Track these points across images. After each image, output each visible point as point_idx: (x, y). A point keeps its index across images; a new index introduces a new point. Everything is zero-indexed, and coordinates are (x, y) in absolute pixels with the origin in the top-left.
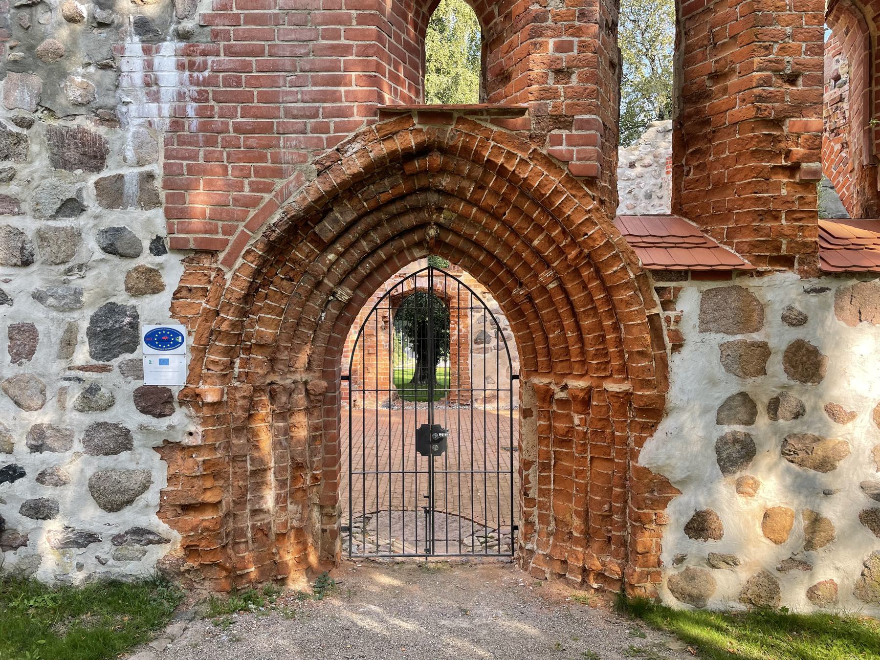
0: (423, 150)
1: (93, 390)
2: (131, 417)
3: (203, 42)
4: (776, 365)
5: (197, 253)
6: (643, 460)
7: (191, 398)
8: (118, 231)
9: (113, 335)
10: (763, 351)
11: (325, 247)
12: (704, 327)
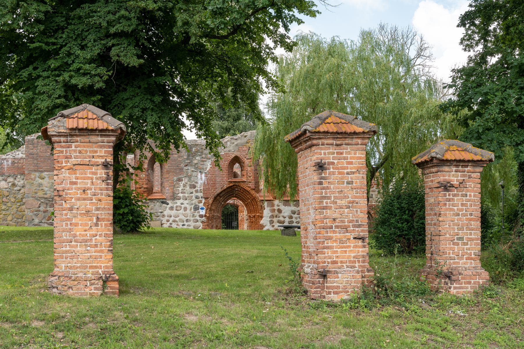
0: (233, 186)
1: (194, 215)
2: (198, 218)
3: (208, 173)
4: (276, 211)
5: (206, 198)
6: (261, 223)
7: (205, 216)
8: (197, 196)
9: (196, 208)
10: (274, 210)
11: (221, 197)
12: (268, 207)
